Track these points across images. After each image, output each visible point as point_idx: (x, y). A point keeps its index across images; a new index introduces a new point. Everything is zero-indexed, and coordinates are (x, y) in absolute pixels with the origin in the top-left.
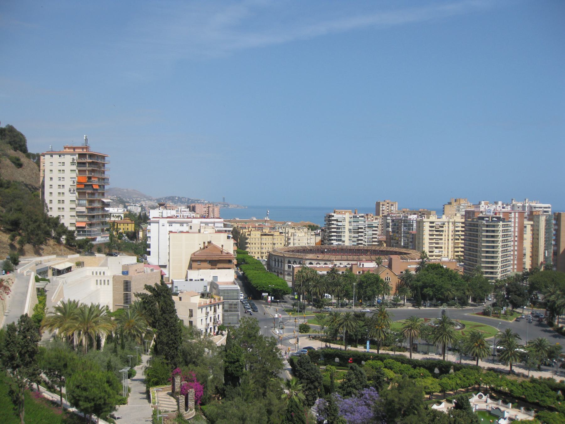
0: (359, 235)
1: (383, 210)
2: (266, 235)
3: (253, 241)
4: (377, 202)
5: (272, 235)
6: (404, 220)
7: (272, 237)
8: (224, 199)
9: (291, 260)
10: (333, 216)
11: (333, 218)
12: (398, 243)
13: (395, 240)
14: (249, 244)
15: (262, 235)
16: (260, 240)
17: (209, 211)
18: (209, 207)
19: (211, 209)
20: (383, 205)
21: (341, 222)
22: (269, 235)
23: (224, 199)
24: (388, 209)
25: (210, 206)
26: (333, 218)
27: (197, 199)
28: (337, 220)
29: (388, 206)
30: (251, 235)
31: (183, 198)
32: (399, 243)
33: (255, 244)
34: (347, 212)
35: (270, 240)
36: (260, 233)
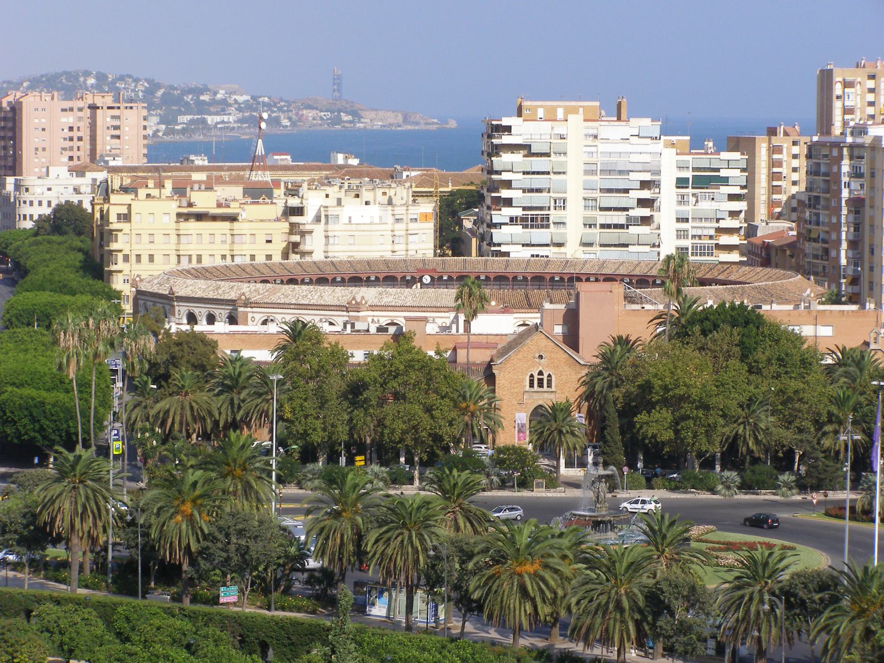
0: (629, 218)
1: (847, 111)
2: (200, 217)
3: (143, 248)
4: (822, 71)
5: (233, 218)
6: (851, 147)
7: (227, 225)
8: (338, 81)
9: (196, 311)
10: (508, 129)
11: (506, 139)
12: (826, 251)
13: (815, 240)
14: (126, 258)
15: (186, 217)
16: (173, 238)
17: (93, 126)
18: (93, 108)
19: (104, 118)
20: (847, 84)
21: (547, 155)
22: (215, 218)
23: (338, 81)
24: (871, 104)
25: (99, 102)
26: (506, 139)
27: (193, 84)
28: (526, 149)
29: (872, 91)
30: (134, 217)
31: (122, 78)
32: (833, 253)
33: (151, 258)
34: (575, 111)
35: (218, 238)
36: (173, 207)
